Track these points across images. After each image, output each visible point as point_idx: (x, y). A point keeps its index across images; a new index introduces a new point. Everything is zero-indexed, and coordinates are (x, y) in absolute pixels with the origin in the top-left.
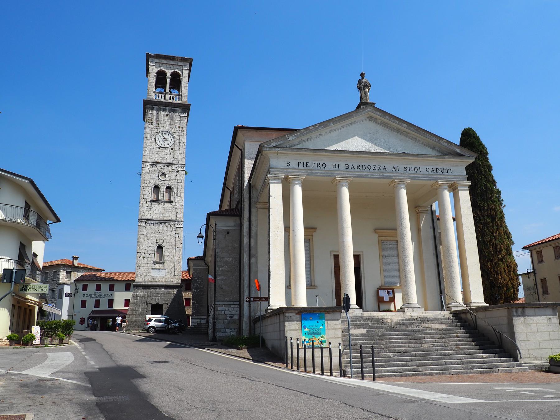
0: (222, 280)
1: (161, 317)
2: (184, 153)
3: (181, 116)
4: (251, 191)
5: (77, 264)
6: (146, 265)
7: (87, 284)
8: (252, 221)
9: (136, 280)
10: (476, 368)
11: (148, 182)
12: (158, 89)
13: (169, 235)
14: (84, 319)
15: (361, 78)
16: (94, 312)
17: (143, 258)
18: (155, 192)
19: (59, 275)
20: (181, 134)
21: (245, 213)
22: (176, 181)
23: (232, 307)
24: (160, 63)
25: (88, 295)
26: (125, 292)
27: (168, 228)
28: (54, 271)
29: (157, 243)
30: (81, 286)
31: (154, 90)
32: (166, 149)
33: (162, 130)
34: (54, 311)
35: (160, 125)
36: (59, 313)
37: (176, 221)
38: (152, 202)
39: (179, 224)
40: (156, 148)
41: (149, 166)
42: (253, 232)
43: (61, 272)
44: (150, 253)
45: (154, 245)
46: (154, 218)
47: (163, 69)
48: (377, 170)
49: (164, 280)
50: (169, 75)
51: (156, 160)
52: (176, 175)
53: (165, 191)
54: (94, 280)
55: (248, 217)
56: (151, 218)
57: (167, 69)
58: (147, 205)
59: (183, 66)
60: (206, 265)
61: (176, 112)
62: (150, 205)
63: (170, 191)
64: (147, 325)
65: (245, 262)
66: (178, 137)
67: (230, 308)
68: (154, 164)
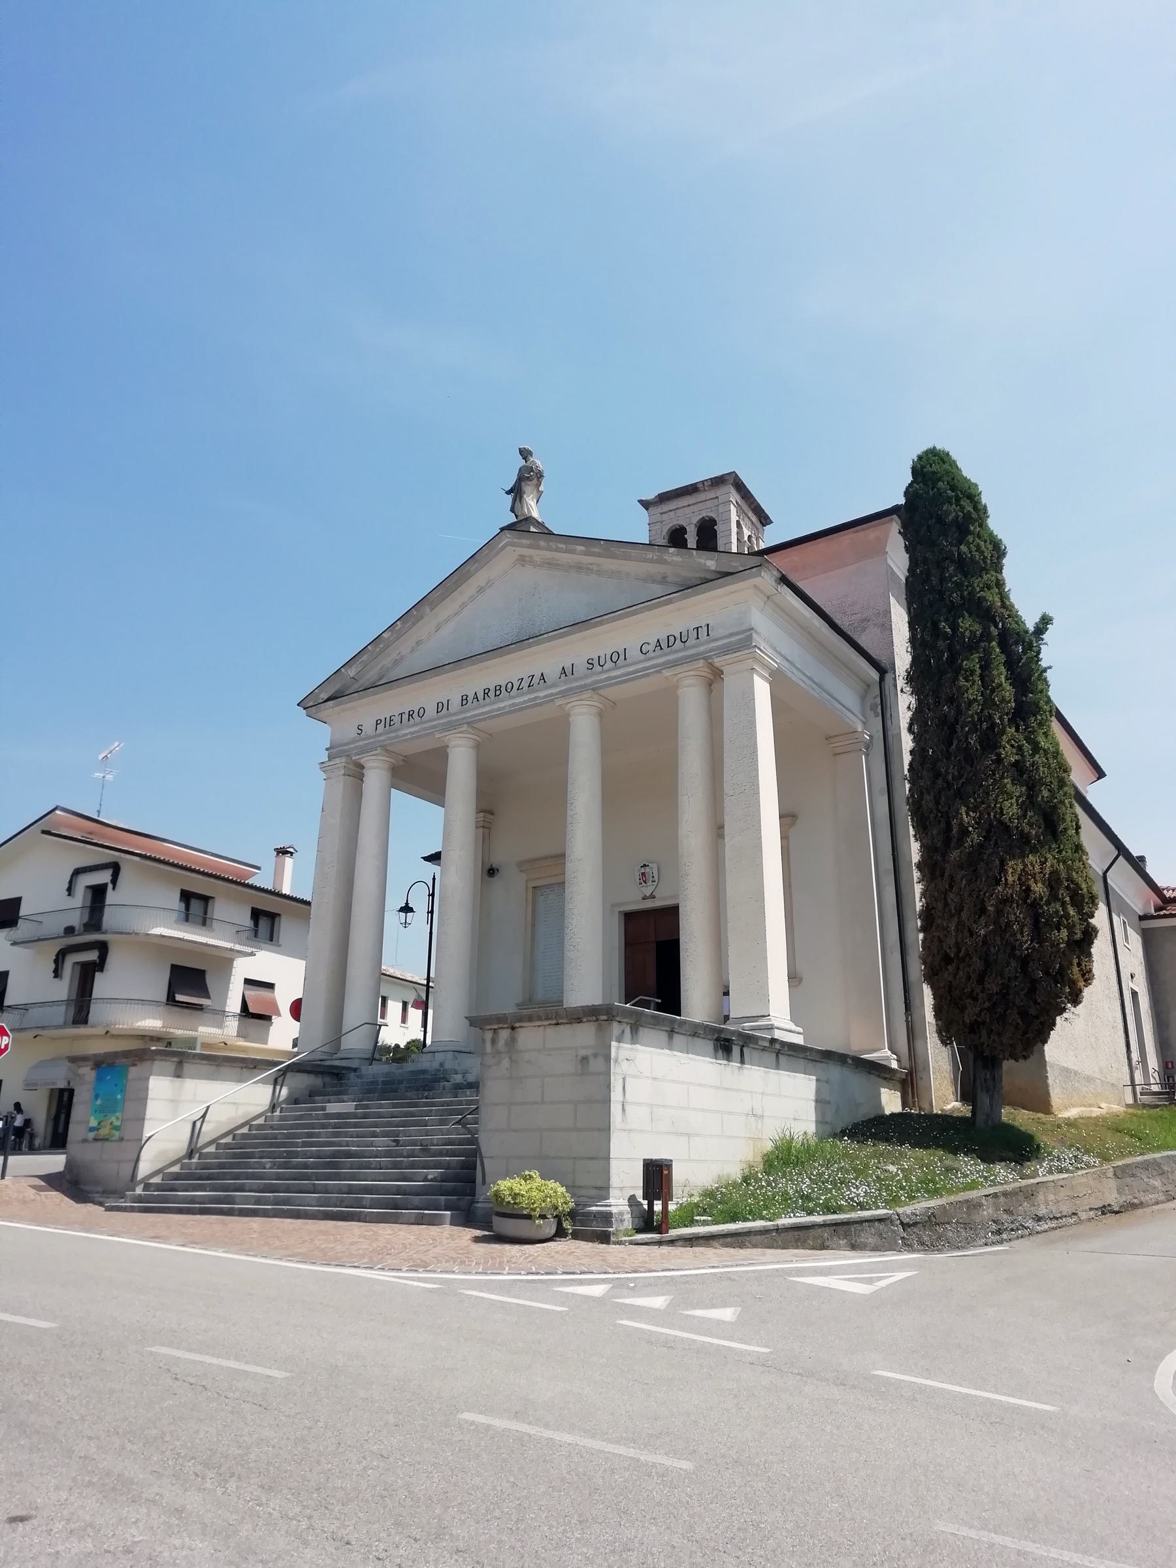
10: (346, 1204)
48: (526, 688)
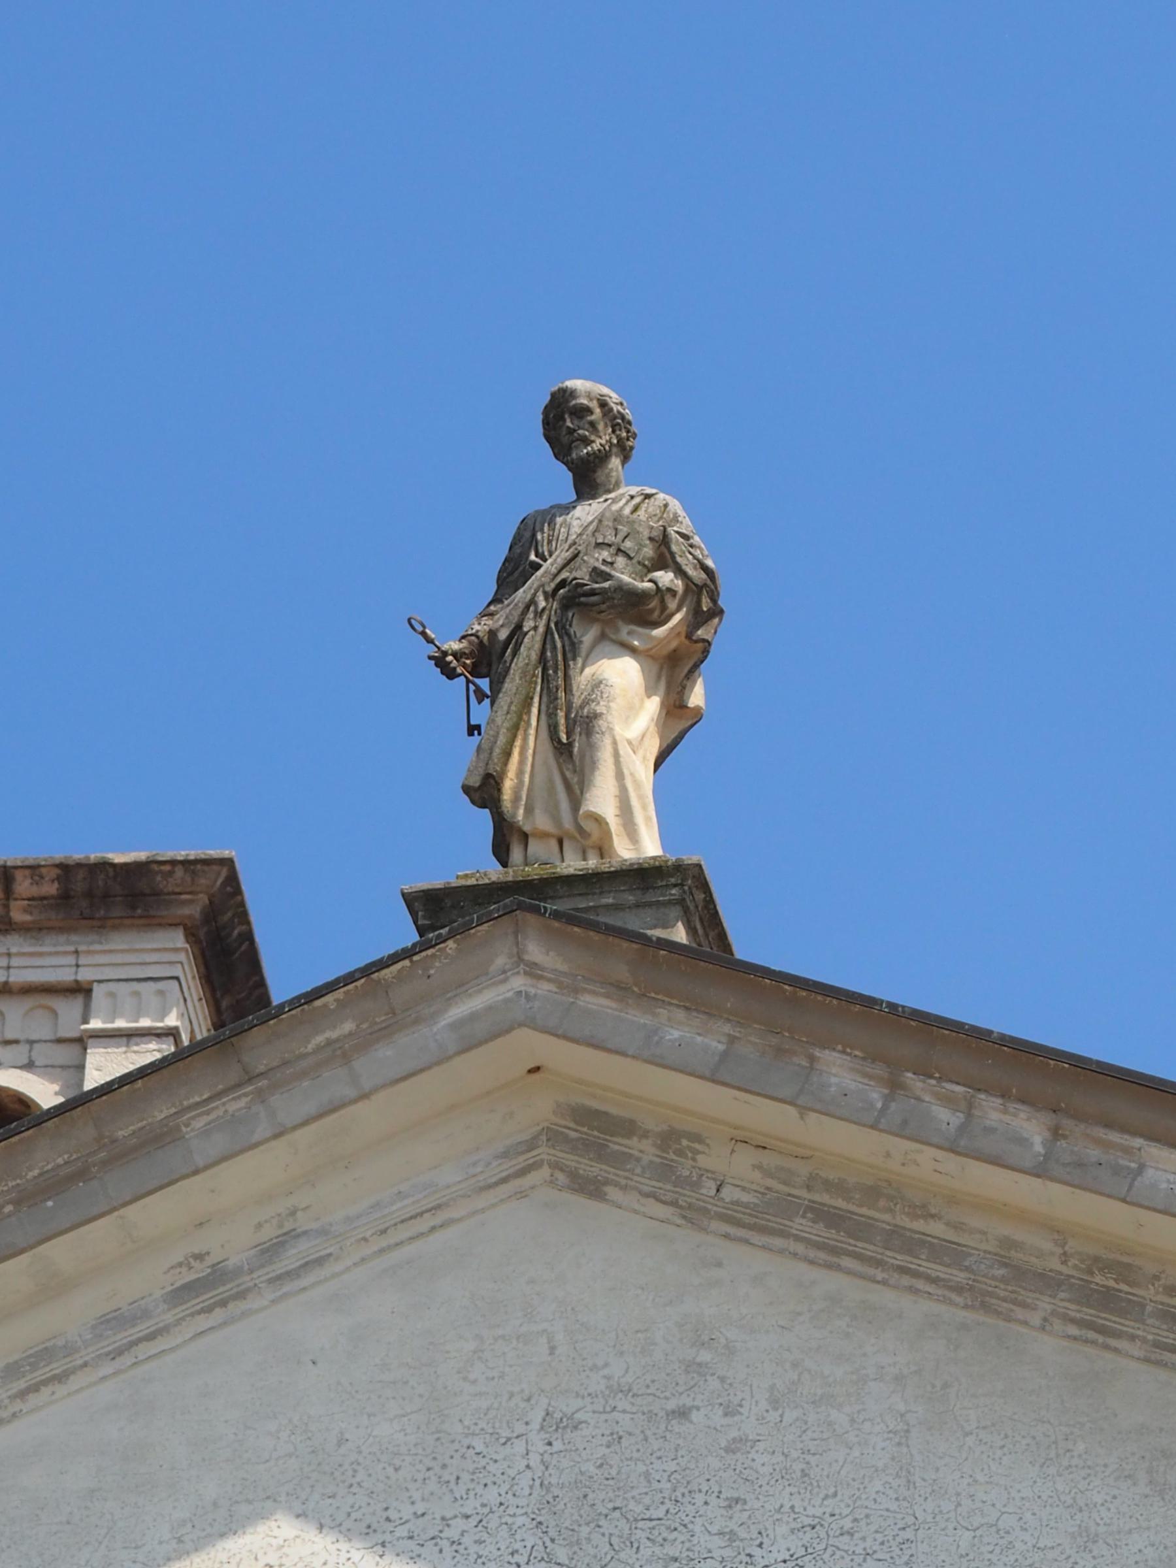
15: (575, 497)
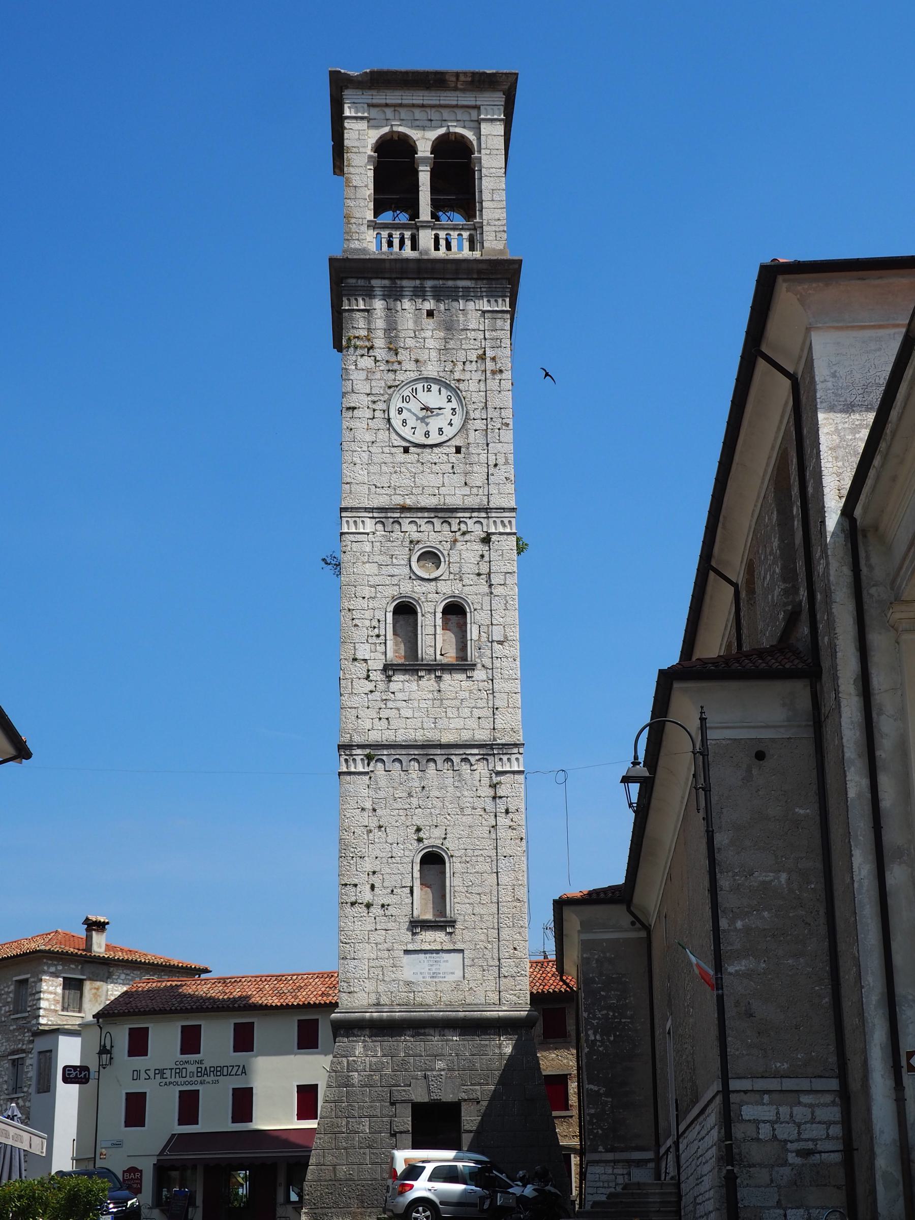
0: (748, 975)
1: (455, 1159)
2: (506, 463)
3: (484, 312)
4: (862, 554)
5: (102, 950)
6: (378, 937)
7: (148, 1028)
8: (876, 692)
9: (345, 1001)
11: (367, 592)
12: (387, 217)
13: (468, 805)
14: (141, 1171)
16: (177, 1142)
17: (368, 906)
18: (399, 631)
19: (37, 997)
20: (493, 384)
21: (839, 655)
22: (483, 580)
23: (805, 1105)
24: (387, 105)
25: (151, 1073)
26: (296, 1054)
27: (460, 775)
28: (15, 979)
29: (420, 840)
30: (121, 1037)
31: (370, 215)
32: (436, 450)
33: (413, 375)
34: (18, 1138)
35: (403, 355)
36: (37, 1146)
37: (491, 746)
38: (391, 673)
39: (505, 758)
40: (394, 450)
41: (369, 526)
42: (885, 741)
43: (44, 984)
44: (394, 883)
45: (407, 853)
46: (400, 738)
47: (401, 129)
49: (456, 997)
50: (424, 149)
51: (398, 500)
52: (482, 556)
53: (439, 622)
54: (171, 1012)
55: (854, 677)
56: (388, 736)
57: (418, 127)
58: (371, 686)
59: (478, 108)
60: (638, 925)
61: (463, 297)
62: (381, 686)
63: (462, 622)
64: (402, 1193)
65: (861, 885)
66: (479, 398)
67: (796, 1110)
68: (389, 515)
